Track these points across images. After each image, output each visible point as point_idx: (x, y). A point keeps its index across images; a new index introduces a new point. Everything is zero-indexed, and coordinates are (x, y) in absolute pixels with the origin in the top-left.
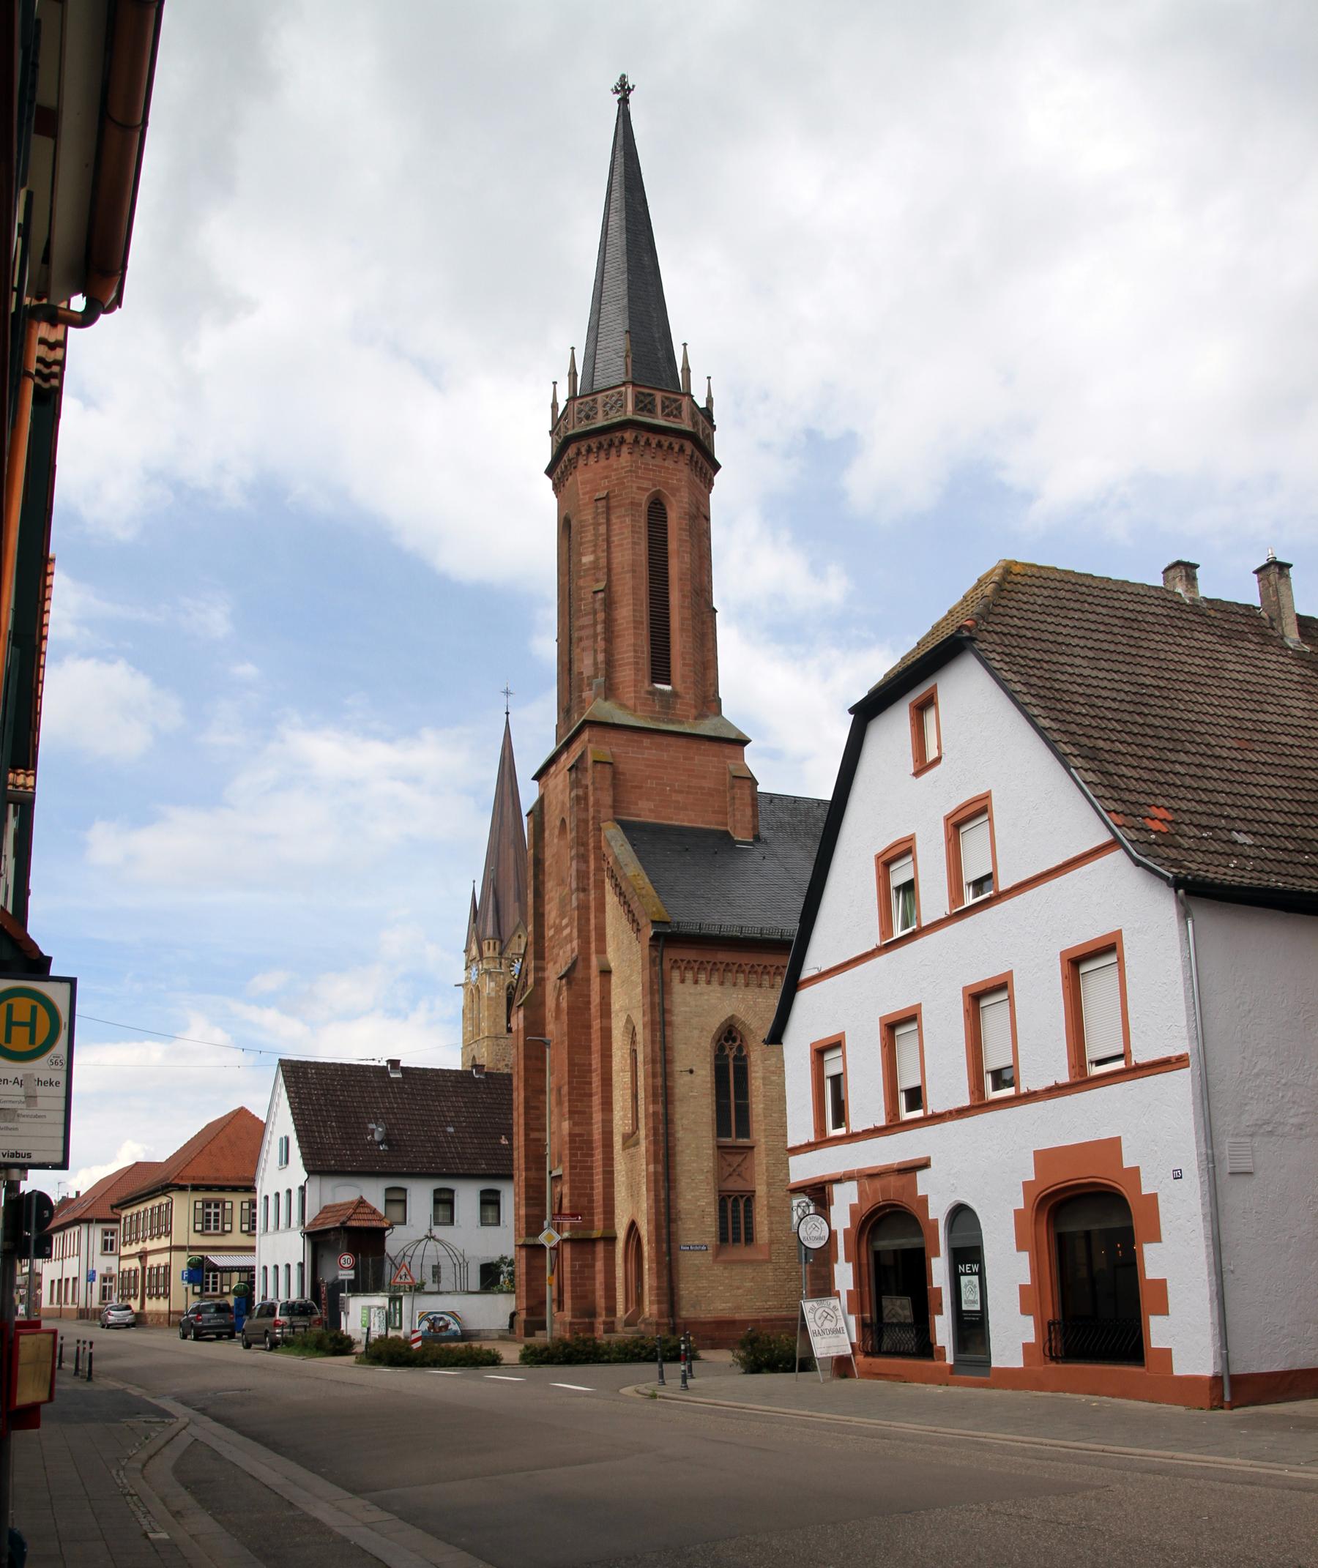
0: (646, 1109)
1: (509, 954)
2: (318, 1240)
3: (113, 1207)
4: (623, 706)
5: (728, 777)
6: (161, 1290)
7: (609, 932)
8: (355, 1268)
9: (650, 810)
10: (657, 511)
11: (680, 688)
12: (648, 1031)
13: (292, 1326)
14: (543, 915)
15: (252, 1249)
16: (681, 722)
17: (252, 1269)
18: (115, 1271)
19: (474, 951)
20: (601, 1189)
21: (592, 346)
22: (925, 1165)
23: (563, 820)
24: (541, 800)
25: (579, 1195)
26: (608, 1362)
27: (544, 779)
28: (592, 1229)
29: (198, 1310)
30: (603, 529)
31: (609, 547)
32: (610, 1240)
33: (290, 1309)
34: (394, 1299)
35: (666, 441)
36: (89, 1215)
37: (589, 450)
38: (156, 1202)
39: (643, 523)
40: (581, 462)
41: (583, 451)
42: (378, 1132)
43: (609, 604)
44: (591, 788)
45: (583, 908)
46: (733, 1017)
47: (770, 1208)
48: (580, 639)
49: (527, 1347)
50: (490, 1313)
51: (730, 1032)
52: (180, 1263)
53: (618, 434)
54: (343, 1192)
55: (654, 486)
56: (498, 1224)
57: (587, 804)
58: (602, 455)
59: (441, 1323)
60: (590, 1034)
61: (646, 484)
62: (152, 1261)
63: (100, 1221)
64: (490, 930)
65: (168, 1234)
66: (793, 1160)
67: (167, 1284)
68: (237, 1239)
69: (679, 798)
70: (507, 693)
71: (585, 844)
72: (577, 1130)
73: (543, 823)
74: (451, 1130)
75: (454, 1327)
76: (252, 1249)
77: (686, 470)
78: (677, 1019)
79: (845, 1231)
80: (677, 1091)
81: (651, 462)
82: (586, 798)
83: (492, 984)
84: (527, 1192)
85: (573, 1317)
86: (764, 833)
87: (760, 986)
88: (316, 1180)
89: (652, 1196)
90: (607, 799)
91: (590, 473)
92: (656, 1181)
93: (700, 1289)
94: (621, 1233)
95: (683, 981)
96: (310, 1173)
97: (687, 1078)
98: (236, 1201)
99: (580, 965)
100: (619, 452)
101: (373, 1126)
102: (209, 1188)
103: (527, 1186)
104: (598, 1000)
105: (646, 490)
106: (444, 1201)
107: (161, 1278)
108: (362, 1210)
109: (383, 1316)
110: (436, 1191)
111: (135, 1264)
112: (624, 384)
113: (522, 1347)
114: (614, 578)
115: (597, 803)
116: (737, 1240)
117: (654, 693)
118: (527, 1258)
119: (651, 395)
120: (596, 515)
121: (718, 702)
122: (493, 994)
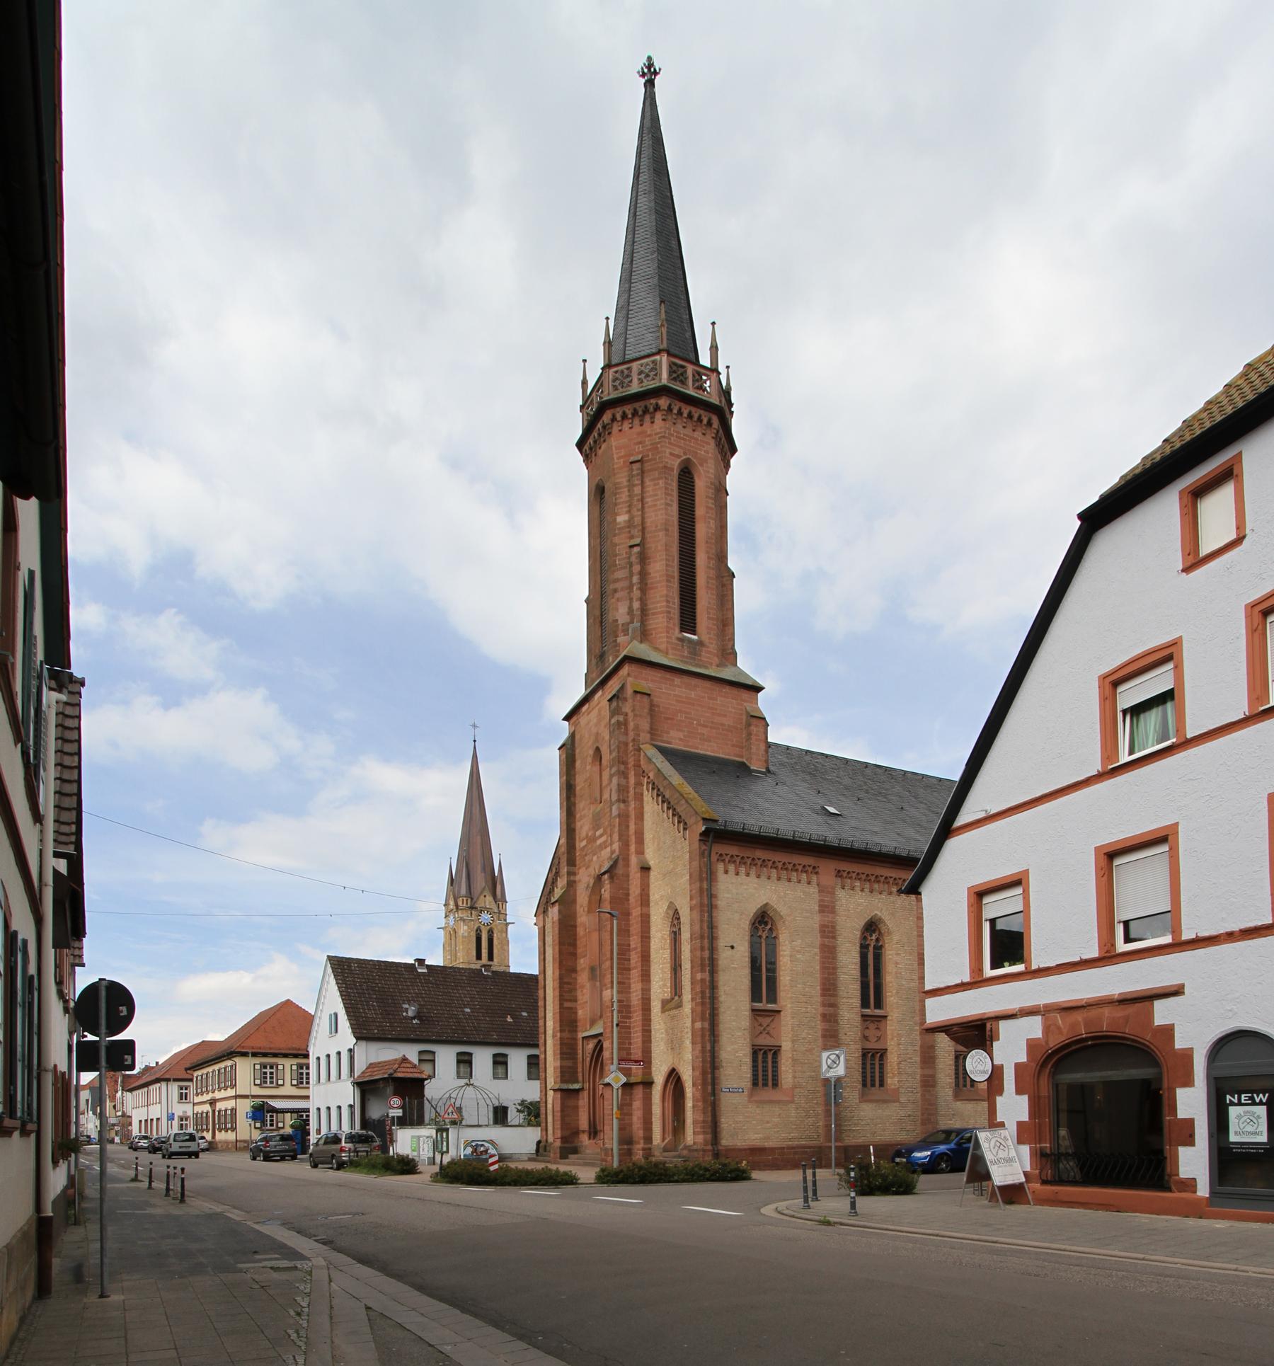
0: (693, 978)
2: (367, 1088)
3: (186, 1069)
4: (656, 649)
5: (744, 717)
6: (229, 1126)
7: (648, 836)
8: (403, 1107)
10: (686, 477)
11: (705, 638)
12: (696, 915)
13: (356, 1151)
14: (574, 830)
15: (307, 1097)
16: (706, 667)
17: (307, 1110)
18: (190, 1113)
19: (452, 903)
20: (640, 1044)
21: (622, 324)
22: (1177, 991)
23: (598, 749)
24: (572, 736)
26: (677, 1181)
27: (574, 718)
29: (266, 1140)
30: (637, 490)
31: (643, 508)
32: (648, 1084)
33: (351, 1138)
34: (442, 1130)
35: (697, 412)
36: (167, 1076)
37: (624, 417)
38: (222, 1065)
39: (675, 485)
40: (615, 428)
41: (619, 417)
42: (412, 1011)
43: (643, 559)
44: (631, 715)
45: (624, 817)
46: (767, 904)
47: (794, 1060)
48: (615, 591)
49: (603, 1170)
50: (518, 1141)
51: (763, 917)
52: (244, 1107)
53: (653, 401)
54: (387, 1053)
55: (685, 454)
56: (506, 1078)
57: (626, 729)
58: (637, 421)
60: (628, 920)
61: (677, 451)
62: (220, 1106)
63: (176, 1080)
64: (463, 891)
65: (234, 1086)
66: (930, 1002)
67: (234, 1121)
68: (288, 1090)
69: (705, 731)
70: (475, 726)
71: (625, 763)
75: (492, 1151)
76: (307, 1097)
77: (712, 442)
78: (721, 902)
79: (1018, 1067)
81: (683, 431)
82: (626, 723)
86: (771, 768)
87: (789, 880)
88: (363, 1044)
89: (699, 1047)
90: (645, 725)
91: (624, 440)
92: (703, 1036)
94: (659, 1077)
95: (726, 872)
96: (358, 1039)
97: (729, 952)
98: (287, 1065)
99: (621, 862)
100: (653, 418)
102: (265, 1055)
104: (638, 891)
105: (679, 457)
106: (465, 1061)
107: (229, 1118)
109: (431, 1144)
111: (207, 1108)
112: (659, 352)
113: (598, 1169)
114: (647, 535)
115: (637, 728)
116: (765, 1085)
117: (682, 640)
119: (683, 367)
120: (631, 477)
121: (734, 654)
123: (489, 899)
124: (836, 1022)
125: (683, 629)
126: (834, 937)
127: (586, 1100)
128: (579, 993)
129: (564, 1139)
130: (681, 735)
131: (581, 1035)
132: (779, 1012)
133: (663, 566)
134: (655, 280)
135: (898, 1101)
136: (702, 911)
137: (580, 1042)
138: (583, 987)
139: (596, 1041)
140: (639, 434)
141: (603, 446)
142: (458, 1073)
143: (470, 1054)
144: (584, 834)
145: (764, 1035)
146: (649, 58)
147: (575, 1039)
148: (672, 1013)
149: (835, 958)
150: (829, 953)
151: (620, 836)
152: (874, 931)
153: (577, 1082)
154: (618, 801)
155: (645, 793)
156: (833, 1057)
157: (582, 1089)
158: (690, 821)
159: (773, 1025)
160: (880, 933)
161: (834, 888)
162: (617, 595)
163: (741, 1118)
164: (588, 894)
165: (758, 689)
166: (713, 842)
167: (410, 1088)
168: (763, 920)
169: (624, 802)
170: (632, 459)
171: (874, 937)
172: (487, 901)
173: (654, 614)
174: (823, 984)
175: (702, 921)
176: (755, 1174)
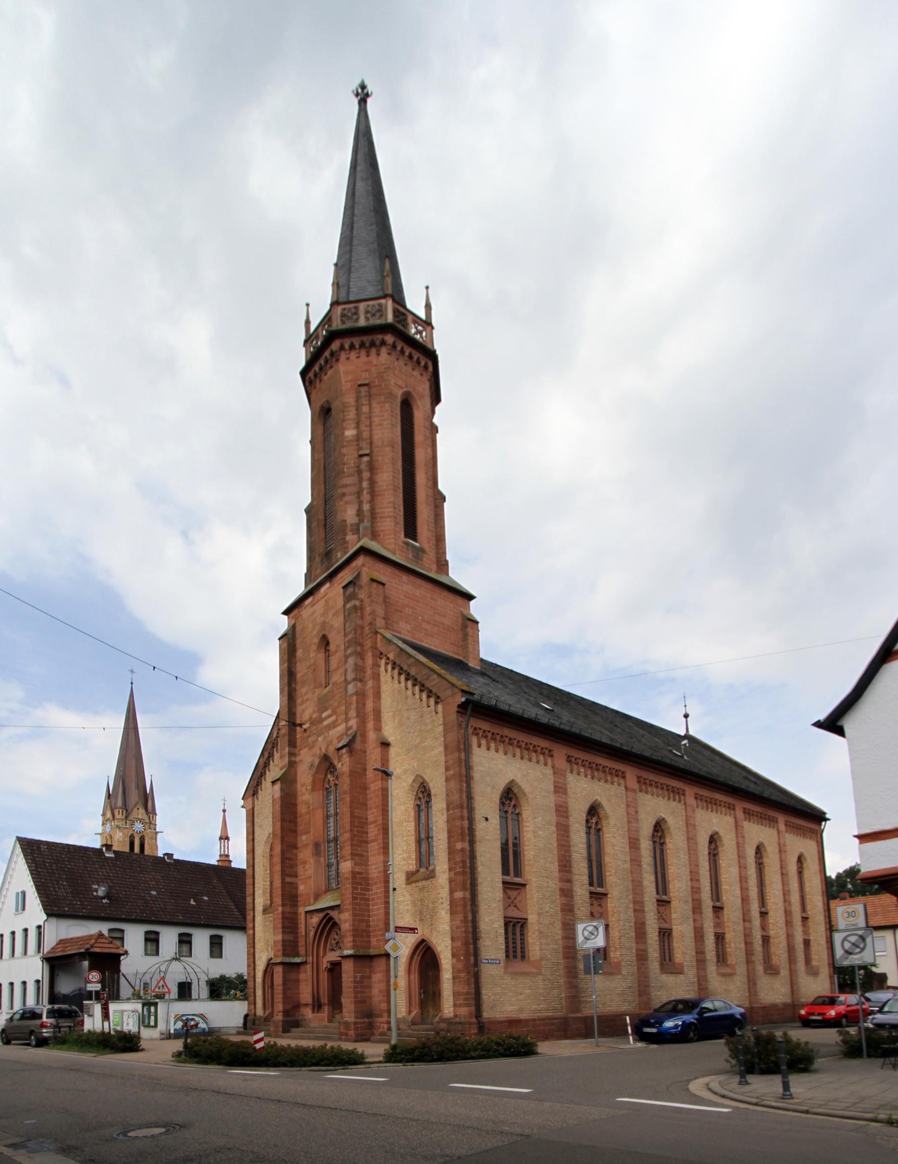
1: (131, 817)
2: (57, 963)
4: (385, 548)
8: (102, 981)
9: (409, 631)
10: (407, 406)
11: (426, 547)
18: (106, 933)
19: (109, 815)
24: (293, 628)
25: (360, 921)
26: (472, 1058)
27: (295, 612)
28: (369, 947)
31: (370, 426)
34: (147, 1004)
35: (416, 355)
37: (352, 347)
40: (343, 356)
41: (347, 346)
42: (101, 891)
44: (367, 601)
45: (361, 695)
46: (513, 781)
47: (541, 933)
48: (344, 495)
53: (380, 337)
55: (406, 386)
57: (362, 614)
58: (363, 352)
59: (193, 1023)
64: (120, 803)
69: (428, 627)
70: (132, 671)
72: (357, 869)
73: (295, 645)
74: (154, 893)
75: (202, 1025)
78: (477, 774)
80: (477, 833)
82: (362, 608)
83: (121, 834)
84: (283, 923)
85: (356, 1018)
88: (54, 921)
89: (460, 917)
90: (380, 611)
91: (349, 368)
92: (465, 906)
93: (495, 994)
94: (402, 947)
95: (479, 746)
99: (358, 738)
101: (96, 887)
103: (283, 918)
105: (401, 387)
108: (101, 940)
109: (136, 1018)
110: (147, 933)
112: (385, 297)
116: (515, 957)
117: (407, 544)
118: (284, 972)
121: (446, 564)
122: (121, 839)
123: (142, 811)
124: (572, 897)
125: (406, 536)
126: (567, 817)
127: (309, 973)
128: (300, 869)
129: (286, 1013)
130: (409, 627)
131: (302, 910)
132: (524, 885)
133: (389, 476)
134: (375, 245)
135: (620, 973)
136: (461, 781)
137: (303, 916)
138: (304, 863)
139: (322, 915)
140: (366, 363)
141: (330, 372)
142: (146, 950)
143: (157, 933)
144: (306, 716)
145: (512, 908)
146: (363, 82)
147: (296, 914)
148: (420, 884)
149: (568, 837)
150: (563, 830)
151: (358, 712)
152: (593, 815)
153: (298, 955)
154: (354, 680)
155: (382, 673)
156: (590, 929)
157: (305, 963)
158: (445, 694)
159: (519, 899)
160: (599, 817)
161: (565, 771)
162: (346, 498)
163: (498, 990)
164: (309, 772)
165: (470, 597)
166: (471, 716)
167: (108, 963)
168: (510, 796)
169: (361, 681)
170: (359, 383)
171: (594, 821)
172: (141, 813)
173: (381, 517)
174: (560, 860)
175: (461, 791)
176: (543, 1047)
